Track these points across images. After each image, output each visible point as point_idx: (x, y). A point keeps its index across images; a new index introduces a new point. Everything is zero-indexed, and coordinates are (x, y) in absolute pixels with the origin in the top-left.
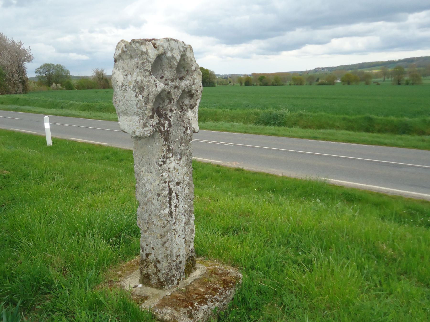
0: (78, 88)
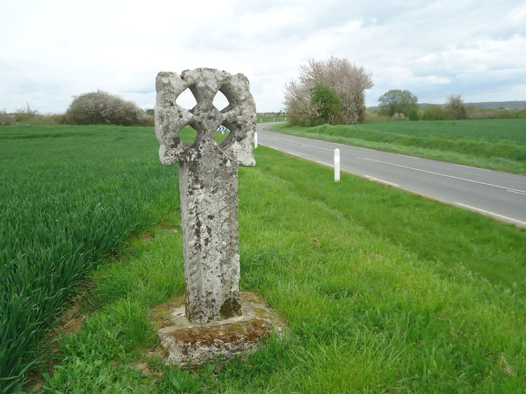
0: (425, 118)
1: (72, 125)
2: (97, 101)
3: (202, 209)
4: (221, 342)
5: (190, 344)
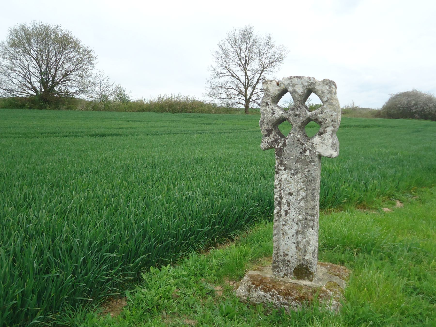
1: (385, 118)
2: (409, 99)
3: (284, 186)
4: (276, 293)
5: (254, 285)
